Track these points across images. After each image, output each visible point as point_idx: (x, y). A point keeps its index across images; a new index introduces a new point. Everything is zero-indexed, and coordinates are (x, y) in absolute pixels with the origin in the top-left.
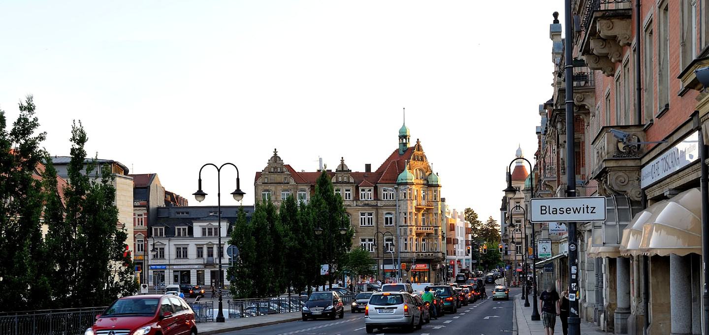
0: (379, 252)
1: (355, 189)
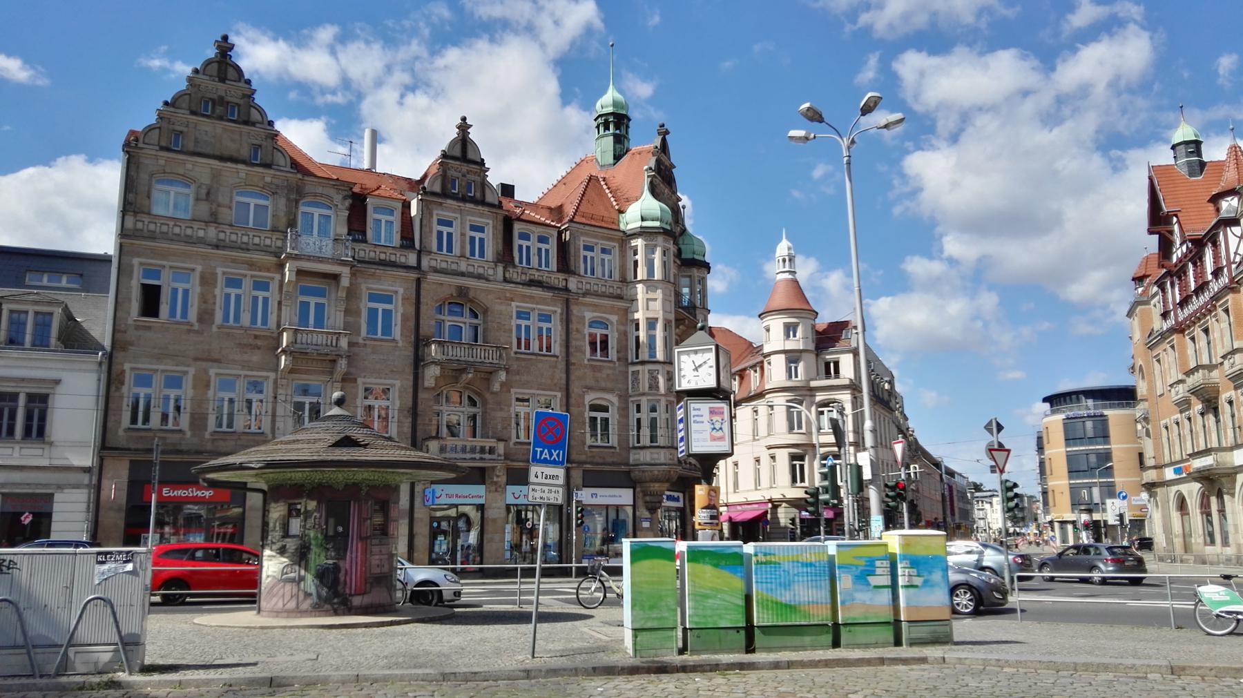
1: (500, 227)
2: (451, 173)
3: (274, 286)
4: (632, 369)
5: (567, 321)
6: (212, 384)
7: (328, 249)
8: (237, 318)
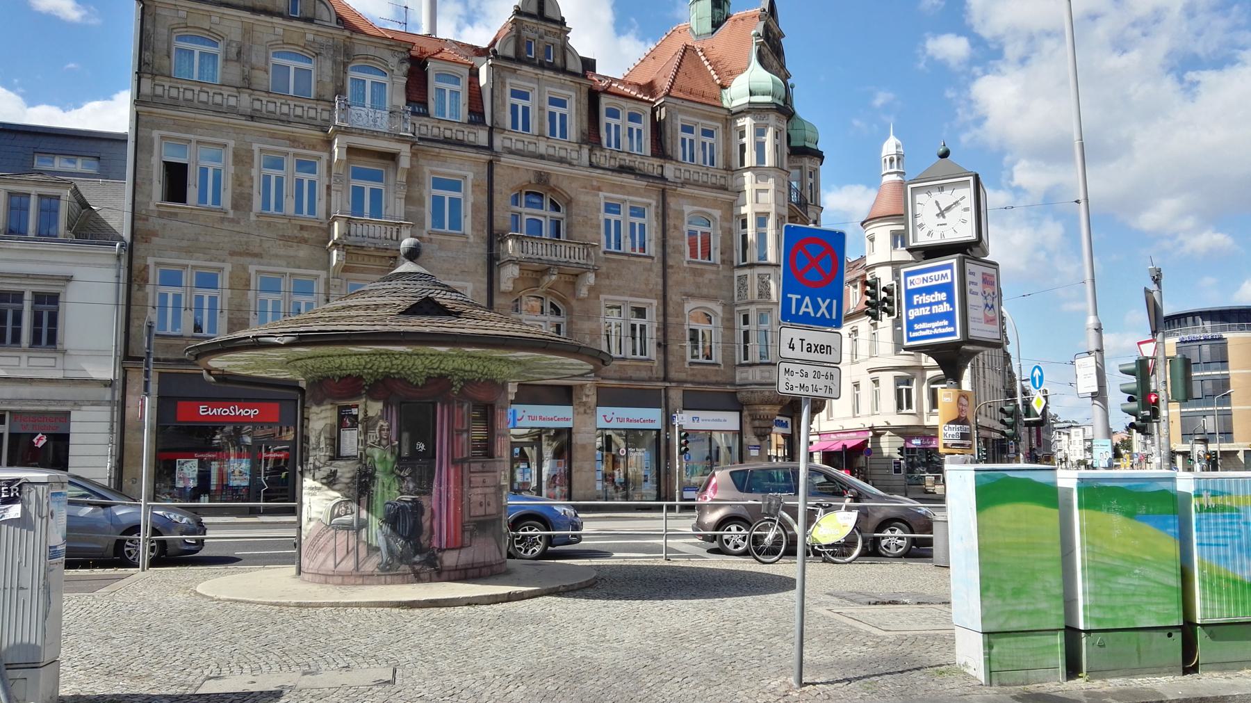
0: (671, 358)
1: (585, 101)
2: (526, 34)
3: (321, 167)
4: (738, 273)
5: (663, 215)
6: (253, 286)
7: (383, 122)
8: (279, 206)
